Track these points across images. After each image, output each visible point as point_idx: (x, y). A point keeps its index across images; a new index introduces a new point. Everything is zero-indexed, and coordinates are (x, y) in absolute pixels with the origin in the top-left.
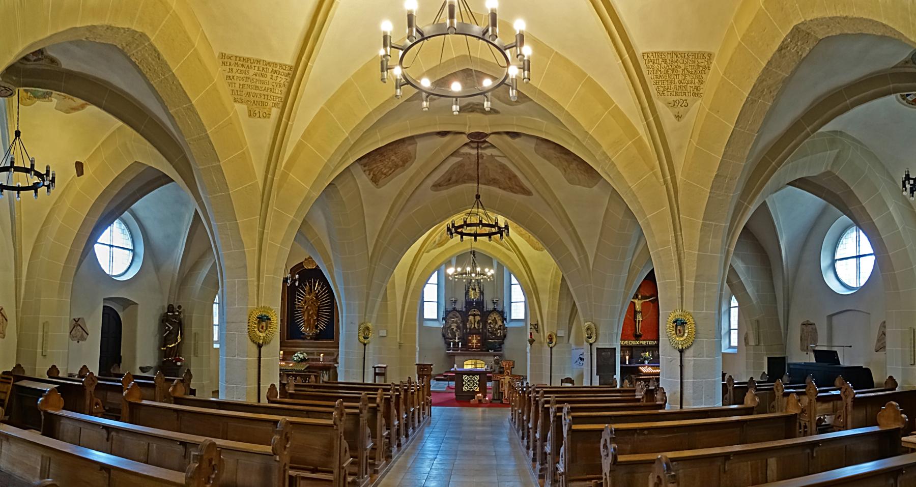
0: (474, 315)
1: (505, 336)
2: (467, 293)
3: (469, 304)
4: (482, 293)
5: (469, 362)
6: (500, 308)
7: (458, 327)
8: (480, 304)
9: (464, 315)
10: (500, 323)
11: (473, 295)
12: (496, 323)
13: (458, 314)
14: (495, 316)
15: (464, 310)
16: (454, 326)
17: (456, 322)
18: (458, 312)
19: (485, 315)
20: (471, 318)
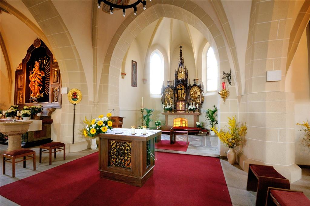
0: (181, 89)
1: (202, 102)
2: (176, 75)
3: (178, 82)
4: (186, 74)
5: (177, 120)
6: (198, 83)
7: (171, 98)
8: (185, 82)
9: (175, 90)
10: (199, 93)
11: (181, 77)
12: (196, 94)
13: (171, 89)
14: (196, 89)
15: (175, 85)
16: (169, 97)
17: (170, 95)
18: (171, 88)
19: (188, 89)
20: (179, 91)
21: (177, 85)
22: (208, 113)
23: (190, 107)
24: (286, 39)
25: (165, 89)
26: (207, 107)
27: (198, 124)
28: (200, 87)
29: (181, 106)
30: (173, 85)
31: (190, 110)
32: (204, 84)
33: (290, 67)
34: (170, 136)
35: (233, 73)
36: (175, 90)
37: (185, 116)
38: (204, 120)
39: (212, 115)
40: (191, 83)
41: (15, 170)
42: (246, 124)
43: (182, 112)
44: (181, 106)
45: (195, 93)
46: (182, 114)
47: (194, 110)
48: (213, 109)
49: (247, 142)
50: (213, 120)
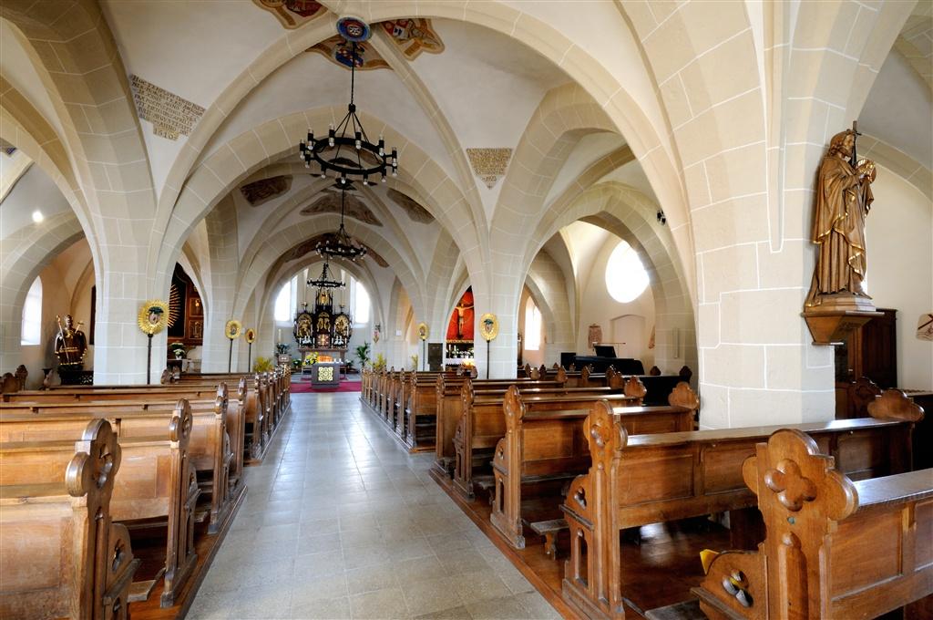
1: (350, 336)
4: (331, 299)
6: (345, 311)
7: (309, 328)
10: (346, 325)
16: (305, 326)
19: (333, 318)
21: (318, 313)
22: (358, 349)
23: (336, 343)
24: (404, 323)
25: (299, 315)
26: (356, 342)
27: (778, 469)
28: (347, 317)
29: (323, 339)
30: (311, 309)
31: (338, 345)
32: (352, 313)
33: (410, 328)
34: (537, 349)
35: (382, 325)
36: (315, 318)
37: (330, 353)
38: (352, 357)
39: (362, 352)
40: (337, 310)
41: (156, 436)
42: (130, 562)
43: (325, 348)
44: (323, 340)
45: (342, 323)
46: (326, 351)
47: (342, 345)
48: (364, 346)
49: (752, 553)
50: (363, 357)
